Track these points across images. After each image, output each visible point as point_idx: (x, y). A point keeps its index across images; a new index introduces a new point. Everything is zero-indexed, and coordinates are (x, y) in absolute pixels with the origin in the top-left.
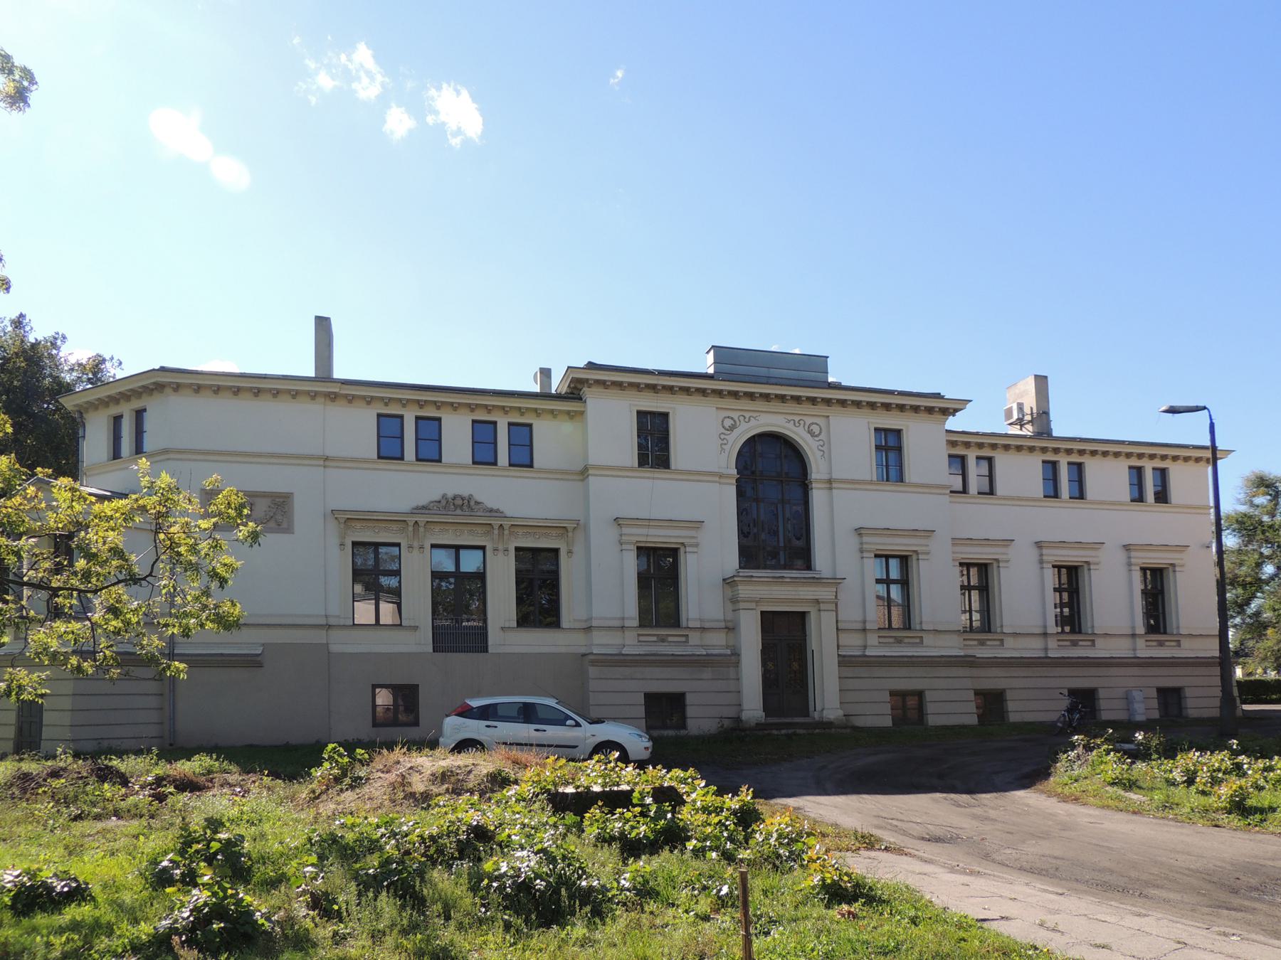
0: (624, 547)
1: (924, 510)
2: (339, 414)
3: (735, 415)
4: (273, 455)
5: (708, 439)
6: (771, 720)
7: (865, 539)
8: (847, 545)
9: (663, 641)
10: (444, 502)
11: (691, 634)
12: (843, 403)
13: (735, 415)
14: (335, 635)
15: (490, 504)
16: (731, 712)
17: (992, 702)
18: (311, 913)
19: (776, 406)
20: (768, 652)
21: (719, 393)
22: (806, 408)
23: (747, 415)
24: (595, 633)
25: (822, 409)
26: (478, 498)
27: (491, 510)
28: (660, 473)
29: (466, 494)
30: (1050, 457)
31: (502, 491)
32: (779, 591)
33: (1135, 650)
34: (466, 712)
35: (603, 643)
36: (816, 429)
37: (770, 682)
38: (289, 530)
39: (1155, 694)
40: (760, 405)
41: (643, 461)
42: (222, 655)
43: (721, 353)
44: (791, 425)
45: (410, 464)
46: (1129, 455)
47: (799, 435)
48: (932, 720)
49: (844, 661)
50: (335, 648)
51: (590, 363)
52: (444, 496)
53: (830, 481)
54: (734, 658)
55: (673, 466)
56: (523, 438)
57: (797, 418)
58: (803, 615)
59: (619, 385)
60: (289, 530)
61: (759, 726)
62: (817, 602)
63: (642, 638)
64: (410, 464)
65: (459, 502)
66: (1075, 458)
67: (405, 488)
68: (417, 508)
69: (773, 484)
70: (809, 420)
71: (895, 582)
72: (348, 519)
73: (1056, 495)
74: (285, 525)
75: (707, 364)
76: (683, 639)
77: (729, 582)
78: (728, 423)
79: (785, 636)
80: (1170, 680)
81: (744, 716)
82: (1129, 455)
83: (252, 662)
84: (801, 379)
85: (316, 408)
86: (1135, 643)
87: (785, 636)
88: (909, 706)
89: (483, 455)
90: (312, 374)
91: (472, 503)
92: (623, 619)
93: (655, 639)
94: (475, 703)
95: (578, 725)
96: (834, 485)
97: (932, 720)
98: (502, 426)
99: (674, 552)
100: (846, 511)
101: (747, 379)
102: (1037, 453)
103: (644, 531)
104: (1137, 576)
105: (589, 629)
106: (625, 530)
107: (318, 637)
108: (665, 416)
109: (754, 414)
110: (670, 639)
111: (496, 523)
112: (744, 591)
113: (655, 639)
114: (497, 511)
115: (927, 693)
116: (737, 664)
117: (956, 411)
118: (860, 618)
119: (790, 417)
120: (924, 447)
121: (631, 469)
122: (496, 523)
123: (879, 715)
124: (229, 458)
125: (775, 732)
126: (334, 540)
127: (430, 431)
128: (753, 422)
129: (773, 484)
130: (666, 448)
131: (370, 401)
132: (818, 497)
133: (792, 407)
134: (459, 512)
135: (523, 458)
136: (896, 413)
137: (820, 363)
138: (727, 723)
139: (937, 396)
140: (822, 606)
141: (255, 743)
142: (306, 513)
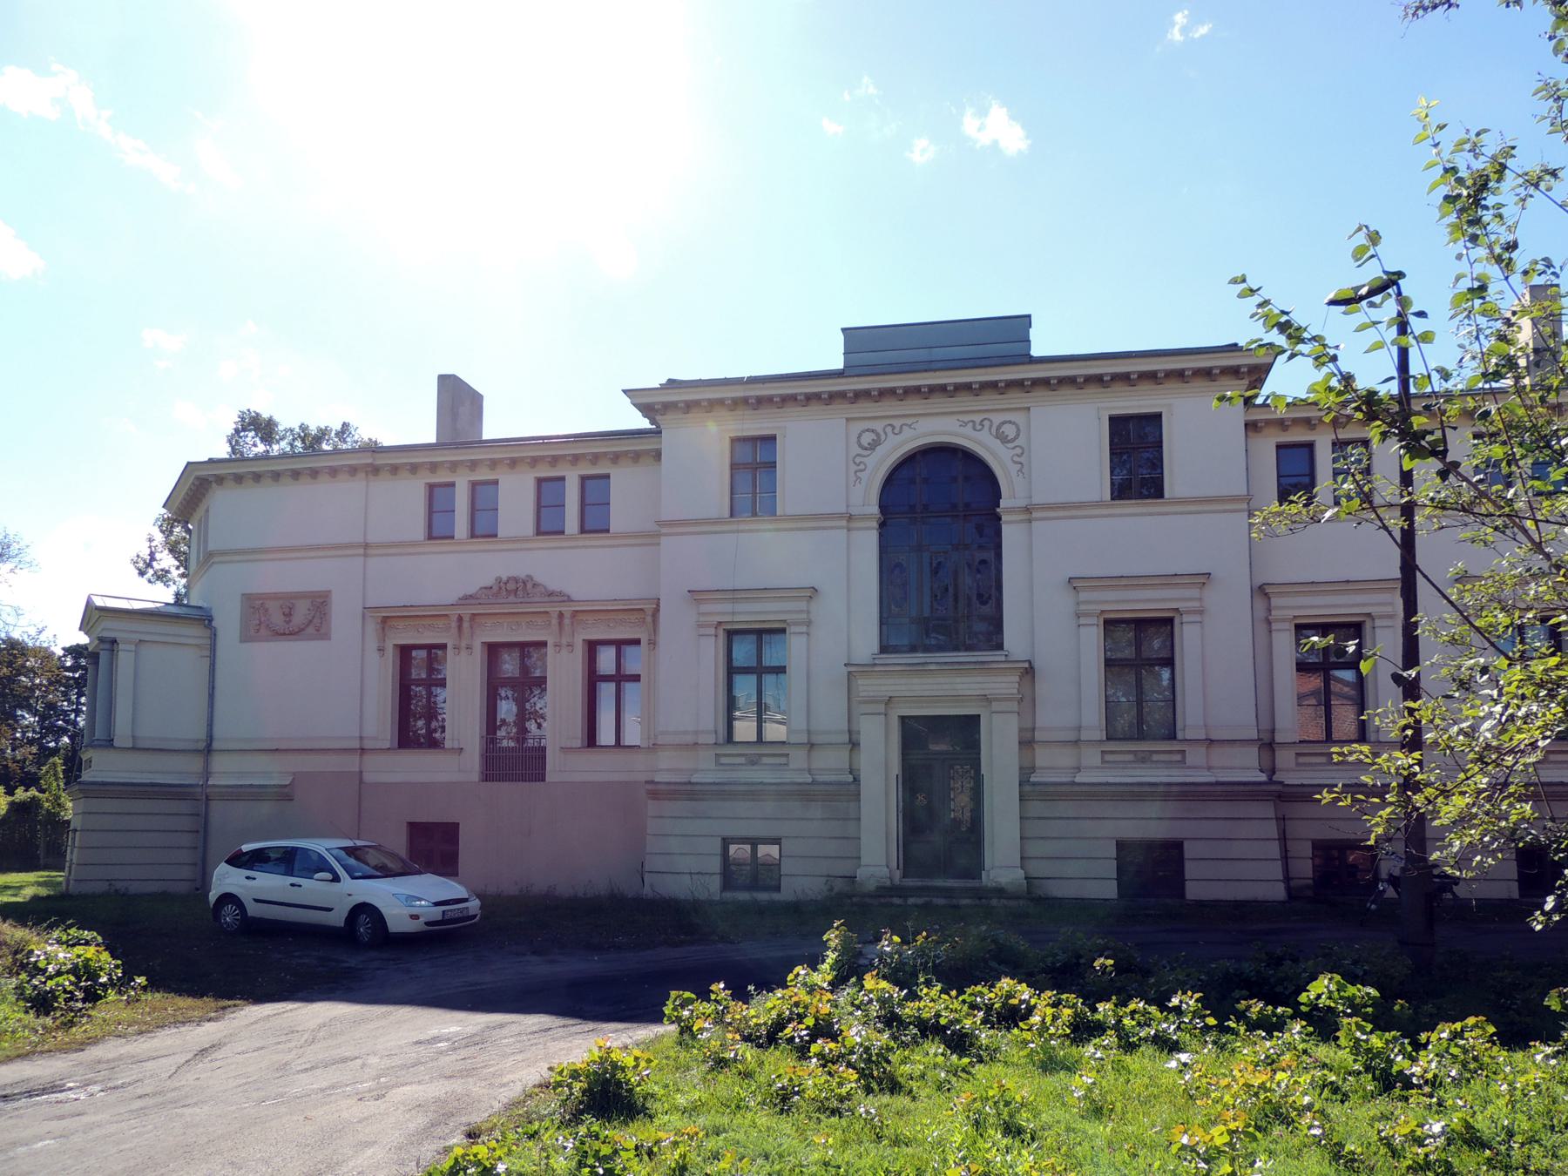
0: (1083, 621)
1: (1210, 540)
2: (383, 488)
3: (878, 426)
4: (311, 548)
5: (837, 469)
6: (910, 882)
9: (753, 763)
10: (495, 589)
12: (1044, 383)
13: (878, 426)
14: (371, 761)
15: (553, 586)
16: (843, 868)
18: (582, 1130)
19: (939, 403)
20: (914, 778)
21: (859, 396)
22: (989, 400)
23: (897, 423)
25: (1016, 398)
26: (538, 578)
27: (551, 594)
28: (1151, 506)
29: (522, 574)
32: (942, 685)
34: (237, 860)
35: (668, 767)
36: (1009, 431)
37: (914, 824)
38: (326, 636)
39: (1112, 852)
40: (914, 405)
41: (1121, 491)
43: (852, 335)
44: (968, 430)
45: (572, 538)
48: (1193, 891)
49: (1030, 791)
51: (671, 381)
53: (1027, 510)
54: (850, 789)
55: (1167, 494)
56: (595, 494)
57: (977, 418)
58: (975, 719)
59: (1070, 381)
61: (886, 891)
63: (1301, 760)
64: (572, 538)
65: (511, 586)
67: (448, 575)
68: (466, 598)
69: (941, 524)
70: (997, 419)
71: (746, 671)
72: (387, 620)
76: (1178, 757)
77: (854, 671)
78: (867, 439)
79: (939, 752)
81: (861, 874)
84: (989, 354)
85: (357, 485)
87: (939, 752)
88: (1154, 870)
89: (547, 526)
90: (432, 439)
91: (529, 586)
92: (696, 733)
93: (742, 760)
94: (246, 848)
95: (336, 879)
97: (1193, 891)
98: (577, 480)
99: (1165, 624)
100: (1061, 556)
101: (958, 364)
103: (728, 607)
105: (811, 746)
106: (1083, 596)
107: (351, 763)
108: (1157, 417)
109: (909, 421)
110: (765, 760)
111: (554, 610)
112: (868, 687)
114: (561, 594)
115: (1186, 844)
118: (190, 729)
119: (966, 418)
120: (1199, 437)
121: (1098, 504)
122: (554, 610)
123: (1093, 877)
124: (280, 556)
125: (897, 901)
126: (372, 643)
127: (483, 500)
128: (907, 433)
129: (941, 524)
130: (1157, 463)
131: (414, 468)
132: (1011, 534)
133: (965, 402)
134: (512, 598)
135: (594, 522)
136: (1145, 387)
137: (1020, 325)
138: (839, 885)
139: (1234, 347)
142: (345, 620)
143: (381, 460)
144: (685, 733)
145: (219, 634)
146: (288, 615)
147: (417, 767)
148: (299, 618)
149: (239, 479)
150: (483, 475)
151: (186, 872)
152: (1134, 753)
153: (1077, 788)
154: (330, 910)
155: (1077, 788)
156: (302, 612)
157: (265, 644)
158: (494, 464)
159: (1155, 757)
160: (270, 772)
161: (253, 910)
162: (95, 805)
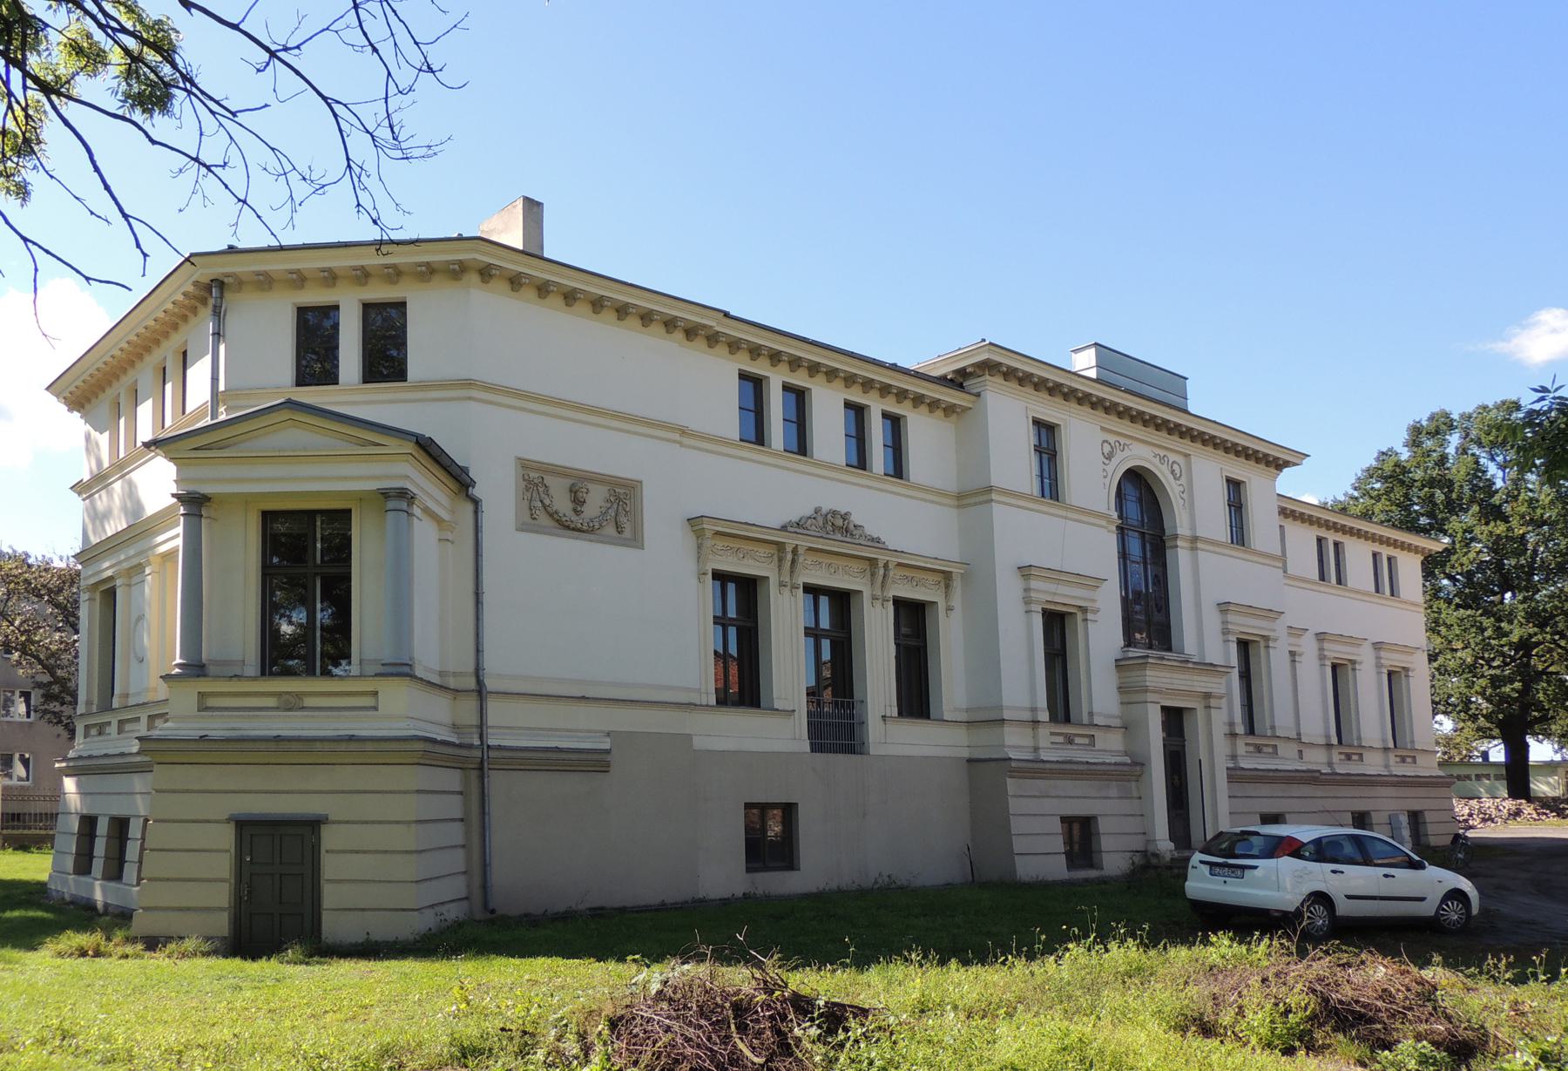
7: (1034, 584)
8: (1212, 621)
9: (1071, 742)
10: (820, 521)
11: (1098, 734)
15: (871, 530)
17: (1081, 836)
24: (1007, 729)
27: (873, 540)
30: (857, 396)
31: (882, 512)
33: (1036, 749)
38: (636, 541)
40: (1137, 430)
42: (557, 750)
46: (850, 380)
47: (1162, 472)
49: (1237, 776)
50: (699, 743)
52: (817, 511)
57: (1162, 453)
60: (636, 541)
62: (1207, 696)
66: (800, 379)
67: (771, 492)
70: (1172, 457)
73: (760, 439)
74: (627, 534)
75: (1085, 363)
78: (1107, 448)
80: (280, 795)
82: (850, 380)
83: (594, 763)
86: (1234, 746)
93: (271, 702)
96: (1199, 545)
98: (885, 410)
102: (839, 384)
103: (1052, 587)
104: (1038, 621)
113: (271, 702)
114: (878, 540)
116: (1138, 778)
117: (1287, 464)
118: (1027, 704)
128: (1127, 453)
131: (734, 346)
138: (1137, 859)
140: (1213, 702)
141: (629, 904)
142: (661, 519)
143: (399, 258)
144: (688, 690)
145: (485, 506)
146: (578, 502)
147: (739, 731)
148: (593, 508)
149: (515, 282)
150: (380, 293)
151: (457, 887)
152: (279, 694)
153: (1041, 766)
154: (1422, 899)
155: (1041, 766)
156: (596, 500)
157: (545, 538)
158: (814, 369)
159: (308, 702)
160: (579, 729)
161: (1344, 908)
162: (95, 782)
